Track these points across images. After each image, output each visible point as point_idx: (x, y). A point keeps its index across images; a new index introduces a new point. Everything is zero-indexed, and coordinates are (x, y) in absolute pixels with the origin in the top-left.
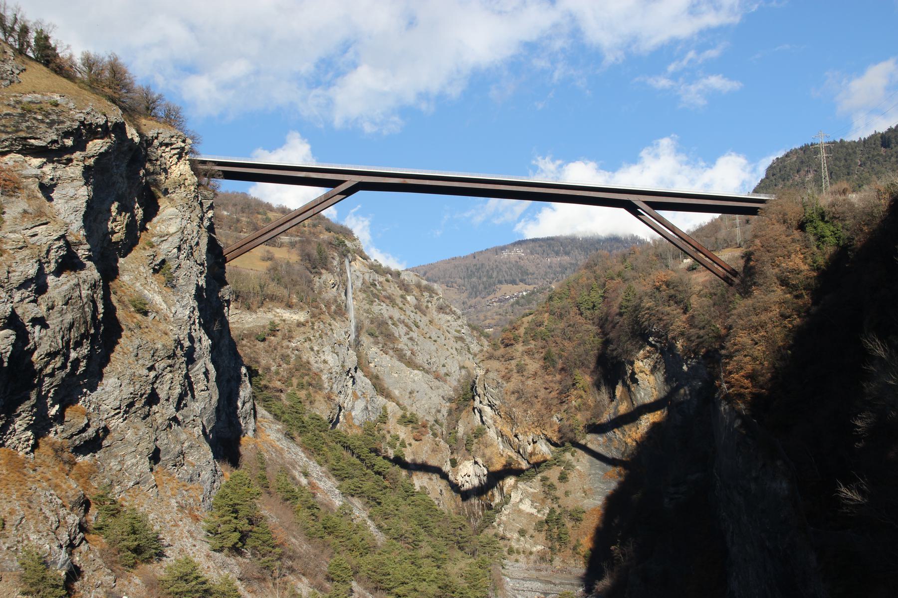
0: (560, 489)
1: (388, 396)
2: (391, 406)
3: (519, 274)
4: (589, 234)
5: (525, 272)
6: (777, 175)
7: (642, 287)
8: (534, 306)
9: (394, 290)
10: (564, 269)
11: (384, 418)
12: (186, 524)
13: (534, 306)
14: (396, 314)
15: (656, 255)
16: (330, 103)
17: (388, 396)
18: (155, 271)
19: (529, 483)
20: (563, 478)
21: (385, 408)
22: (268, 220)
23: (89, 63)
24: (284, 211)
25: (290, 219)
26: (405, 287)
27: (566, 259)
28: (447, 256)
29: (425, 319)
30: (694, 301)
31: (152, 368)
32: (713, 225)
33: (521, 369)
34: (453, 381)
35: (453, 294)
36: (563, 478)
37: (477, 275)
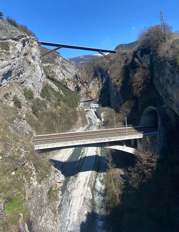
0: (88, 89)
1: (65, 76)
2: (65, 77)
3: (82, 60)
4: (134, 142)
5: (83, 60)
6: (117, 48)
7: (99, 62)
8: (85, 64)
9: (66, 61)
10: (89, 59)
11: (64, 79)
12: (37, 93)
13: (85, 64)
14: (66, 65)
15: (101, 58)
16: (15, 173)
17: (65, 76)
18: (32, 58)
19: (98, 155)
20: (88, 87)
21: (65, 78)
22: (48, 51)
23: (22, 26)
24: (50, 50)
25: (51, 51)
26: (67, 61)
27: (89, 58)
28: (73, 57)
29: (70, 66)
30: (106, 64)
31: (32, 71)
32: (109, 54)
33: (83, 73)
34: (74, 74)
35: (74, 62)
36: (88, 87)
37: (77, 60)
